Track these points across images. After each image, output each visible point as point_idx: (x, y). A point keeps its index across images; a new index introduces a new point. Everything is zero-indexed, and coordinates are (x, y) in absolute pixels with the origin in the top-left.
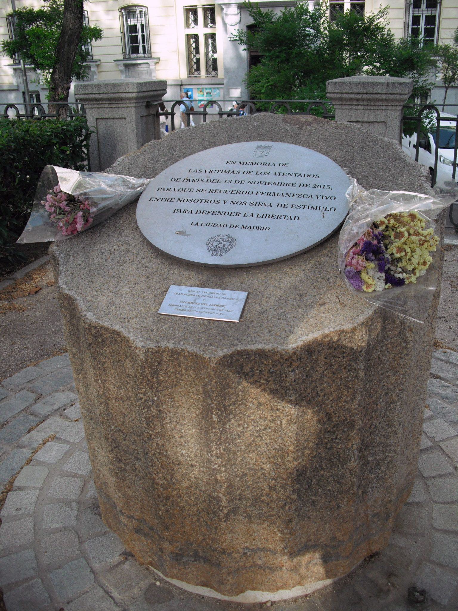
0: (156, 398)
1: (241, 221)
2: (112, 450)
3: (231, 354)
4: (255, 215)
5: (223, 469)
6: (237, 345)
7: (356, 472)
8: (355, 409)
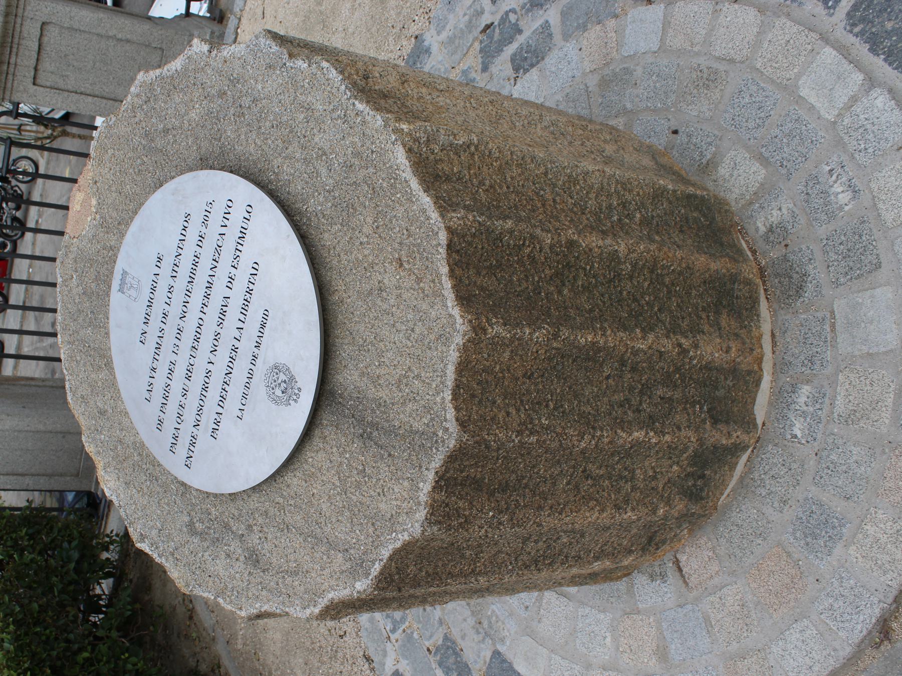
0: (491, 514)
1: (246, 346)
2: (539, 570)
3: (455, 409)
4: (240, 325)
5: (598, 433)
6: (443, 398)
7: (632, 244)
8: (553, 239)
